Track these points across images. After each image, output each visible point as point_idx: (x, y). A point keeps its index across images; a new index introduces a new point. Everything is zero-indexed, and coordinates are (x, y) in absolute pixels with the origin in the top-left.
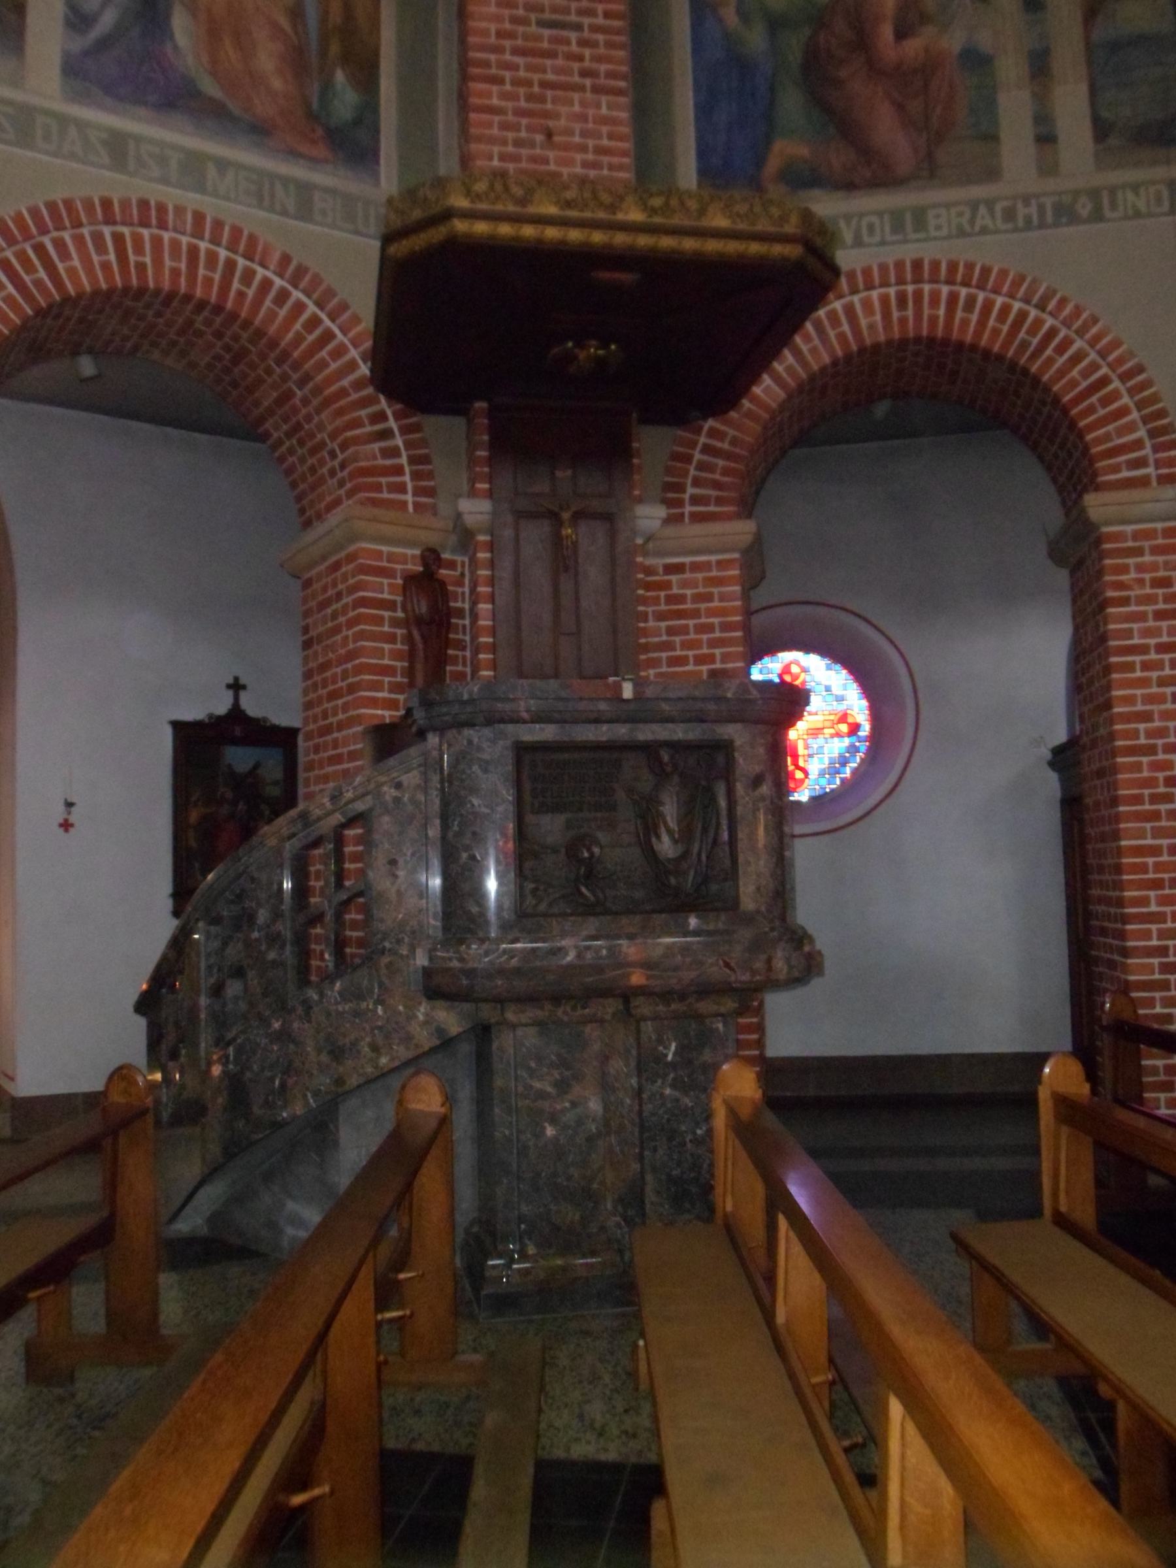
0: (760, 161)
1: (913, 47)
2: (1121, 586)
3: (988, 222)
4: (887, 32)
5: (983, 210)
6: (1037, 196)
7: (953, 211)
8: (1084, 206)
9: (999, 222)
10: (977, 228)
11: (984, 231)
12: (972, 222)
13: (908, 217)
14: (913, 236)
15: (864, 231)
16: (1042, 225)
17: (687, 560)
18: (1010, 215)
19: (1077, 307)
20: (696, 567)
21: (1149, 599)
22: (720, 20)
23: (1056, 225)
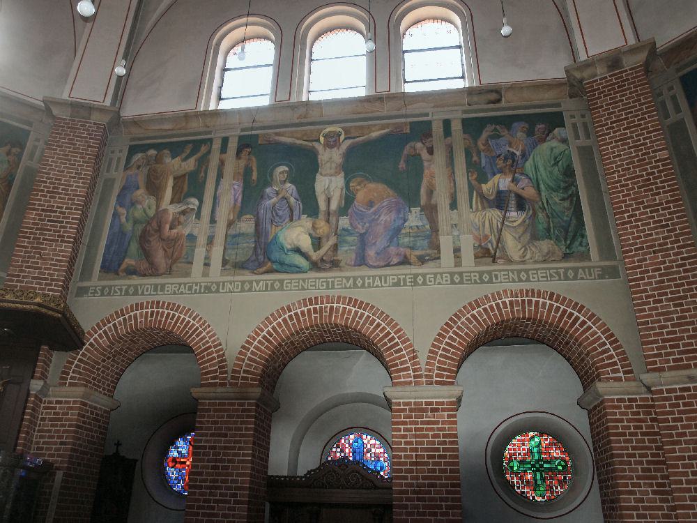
0: (120, 265)
1: (174, 231)
2: (201, 422)
3: (583, 275)
4: (168, 226)
5: (182, 286)
6: (200, 283)
7: (173, 286)
8: (486, 277)
9: (588, 276)
10: (375, 285)
11: (182, 293)
12: (178, 290)
13: (159, 287)
14: (159, 293)
15: (145, 290)
16: (200, 293)
17: (64, 399)
18: (127, 291)
19: (205, 321)
20: (66, 402)
21: (210, 429)
22: (120, 221)
23: (204, 293)
